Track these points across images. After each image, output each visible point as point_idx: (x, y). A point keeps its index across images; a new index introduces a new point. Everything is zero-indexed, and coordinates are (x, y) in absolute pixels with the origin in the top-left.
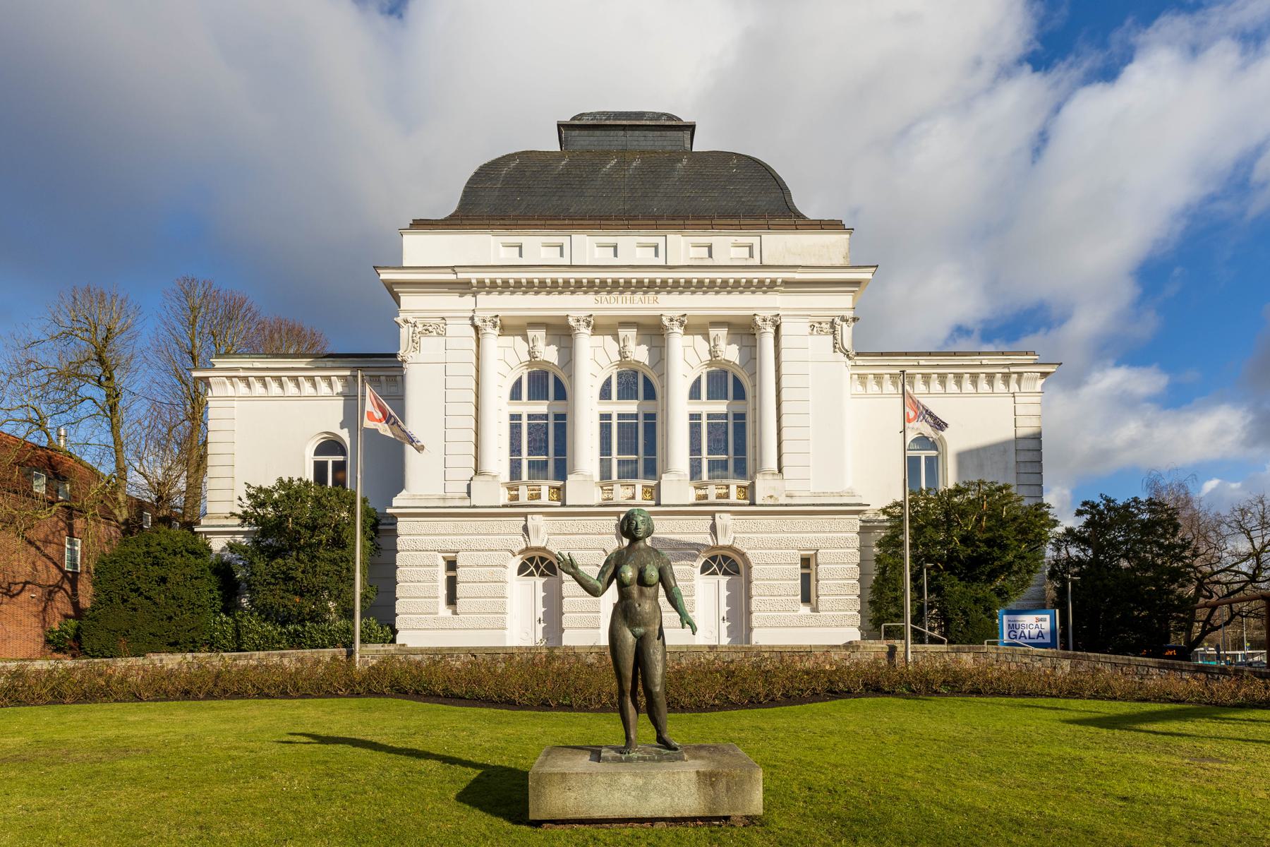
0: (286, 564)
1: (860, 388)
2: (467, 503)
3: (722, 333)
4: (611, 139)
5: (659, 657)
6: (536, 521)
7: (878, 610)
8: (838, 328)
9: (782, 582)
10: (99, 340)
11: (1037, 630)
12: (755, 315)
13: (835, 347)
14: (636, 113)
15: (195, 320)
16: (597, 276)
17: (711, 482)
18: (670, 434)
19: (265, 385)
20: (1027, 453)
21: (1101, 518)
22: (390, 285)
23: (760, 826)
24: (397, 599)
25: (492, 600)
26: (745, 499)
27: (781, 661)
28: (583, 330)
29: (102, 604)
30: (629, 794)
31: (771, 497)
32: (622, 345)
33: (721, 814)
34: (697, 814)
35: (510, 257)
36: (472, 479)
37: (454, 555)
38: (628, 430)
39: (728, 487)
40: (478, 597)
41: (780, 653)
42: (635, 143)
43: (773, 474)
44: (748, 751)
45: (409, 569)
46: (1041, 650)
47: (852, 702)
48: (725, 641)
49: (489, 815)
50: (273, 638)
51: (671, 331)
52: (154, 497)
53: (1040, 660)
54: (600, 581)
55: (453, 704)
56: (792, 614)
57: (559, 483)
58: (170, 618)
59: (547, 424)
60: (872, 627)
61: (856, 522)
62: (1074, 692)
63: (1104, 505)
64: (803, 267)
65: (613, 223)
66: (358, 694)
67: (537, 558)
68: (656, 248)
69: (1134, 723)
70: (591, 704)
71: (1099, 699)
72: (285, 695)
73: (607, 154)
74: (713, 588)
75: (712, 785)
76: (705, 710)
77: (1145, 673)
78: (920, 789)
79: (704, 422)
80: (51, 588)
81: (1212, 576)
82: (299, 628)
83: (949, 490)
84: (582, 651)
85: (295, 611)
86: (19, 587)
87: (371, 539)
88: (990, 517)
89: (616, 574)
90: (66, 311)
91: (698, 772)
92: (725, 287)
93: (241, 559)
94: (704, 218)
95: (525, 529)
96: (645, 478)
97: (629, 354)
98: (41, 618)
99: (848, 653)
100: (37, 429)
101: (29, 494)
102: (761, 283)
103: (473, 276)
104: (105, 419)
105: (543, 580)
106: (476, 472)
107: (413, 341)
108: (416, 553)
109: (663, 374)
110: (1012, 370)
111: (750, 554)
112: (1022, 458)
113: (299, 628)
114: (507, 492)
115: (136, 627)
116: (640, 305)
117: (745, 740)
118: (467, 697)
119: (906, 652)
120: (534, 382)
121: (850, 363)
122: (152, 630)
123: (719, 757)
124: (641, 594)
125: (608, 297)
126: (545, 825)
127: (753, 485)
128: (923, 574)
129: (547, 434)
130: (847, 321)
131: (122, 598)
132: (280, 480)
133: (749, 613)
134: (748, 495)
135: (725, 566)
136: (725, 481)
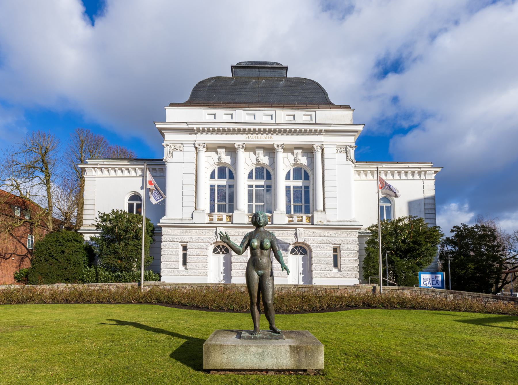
0: (115, 246)
1: (358, 176)
2: (191, 222)
3: (299, 152)
4: (253, 72)
5: (271, 286)
7: (367, 271)
8: (349, 150)
9: (325, 258)
10: (43, 153)
12: (313, 144)
13: (347, 158)
14: (263, 62)
15: (82, 146)
16: (247, 127)
17: (295, 214)
18: (277, 201)
19: (108, 171)
20: (429, 205)
21: (462, 233)
22: (160, 130)
23: (323, 375)
24: (161, 262)
26: (309, 222)
27: (326, 292)
28: (241, 150)
29: (37, 262)
30: (255, 357)
31: (320, 221)
32: (257, 156)
33: (302, 368)
34: (290, 368)
35: (211, 118)
36: (193, 212)
37: (186, 244)
39: (302, 217)
40: (195, 262)
41: (326, 289)
42: (263, 74)
43: (321, 212)
44: (313, 333)
45: (167, 249)
46: (440, 289)
47: (358, 311)
48: (301, 283)
49: (184, 365)
50: (109, 278)
51: (278, 151)
52: (64, 218)
53: (440, 294)
54: (241, 247)
55: (181, 308)
57: (230, 214)
58: (66, 269)
60: (364, 278)
61: (357, 233)
62: (457, 308)
63: (463, 228)
64: (333, 124)
65: (254, 105)
66: (141, 303)
68: (272, 116)
69: (492, 322)
70: (242, 310)
71: (468, 312)
72: (109, 302)
73: (251, 78)
75: (298, 352)
76: (293, 313)
77: (487, 300)
78: (401, 356)
80: (23, 256)
81: (506, 260)
83: (396, 220)
84: (239, 286)
85: (118, 267)
86: (9, 256)
87: (151, 236)
88: (414, 232)
89: (249, 244)
90: (29, 140)
91: (290, 346)
92: (300, 132)
93: (96, 244)
94: (292, 104)
97: (260, 160)
98: (18, 268)
99: (355, 289)
100: (16, 189)
101: (12, 216)
102: (316, 131)
103: (195, 127)
104: (44, 185)
105: (224, 255)
107: (170, 153)
108: (170, 243)
109: (274, 169)
110: (422, 169)
111: (311, 246)
112: (426, 207)
115: (51, 272)
116: (265, 140)
117: (311, 328)
118: (188, 305)
119: (380, 289)
121: (353, 165)
122: (58, 274)
123: (301, 338)
124: (262, 253)
125: (251, 136)
126: (212, 372)
127: (313, 216)
128: (386, 256)
130: (352, 147)
131: (46, 259)
132: (113, 210)
133: (311, 271)
134: (311, 220)
135: (301, 251)
136: (301, 214)
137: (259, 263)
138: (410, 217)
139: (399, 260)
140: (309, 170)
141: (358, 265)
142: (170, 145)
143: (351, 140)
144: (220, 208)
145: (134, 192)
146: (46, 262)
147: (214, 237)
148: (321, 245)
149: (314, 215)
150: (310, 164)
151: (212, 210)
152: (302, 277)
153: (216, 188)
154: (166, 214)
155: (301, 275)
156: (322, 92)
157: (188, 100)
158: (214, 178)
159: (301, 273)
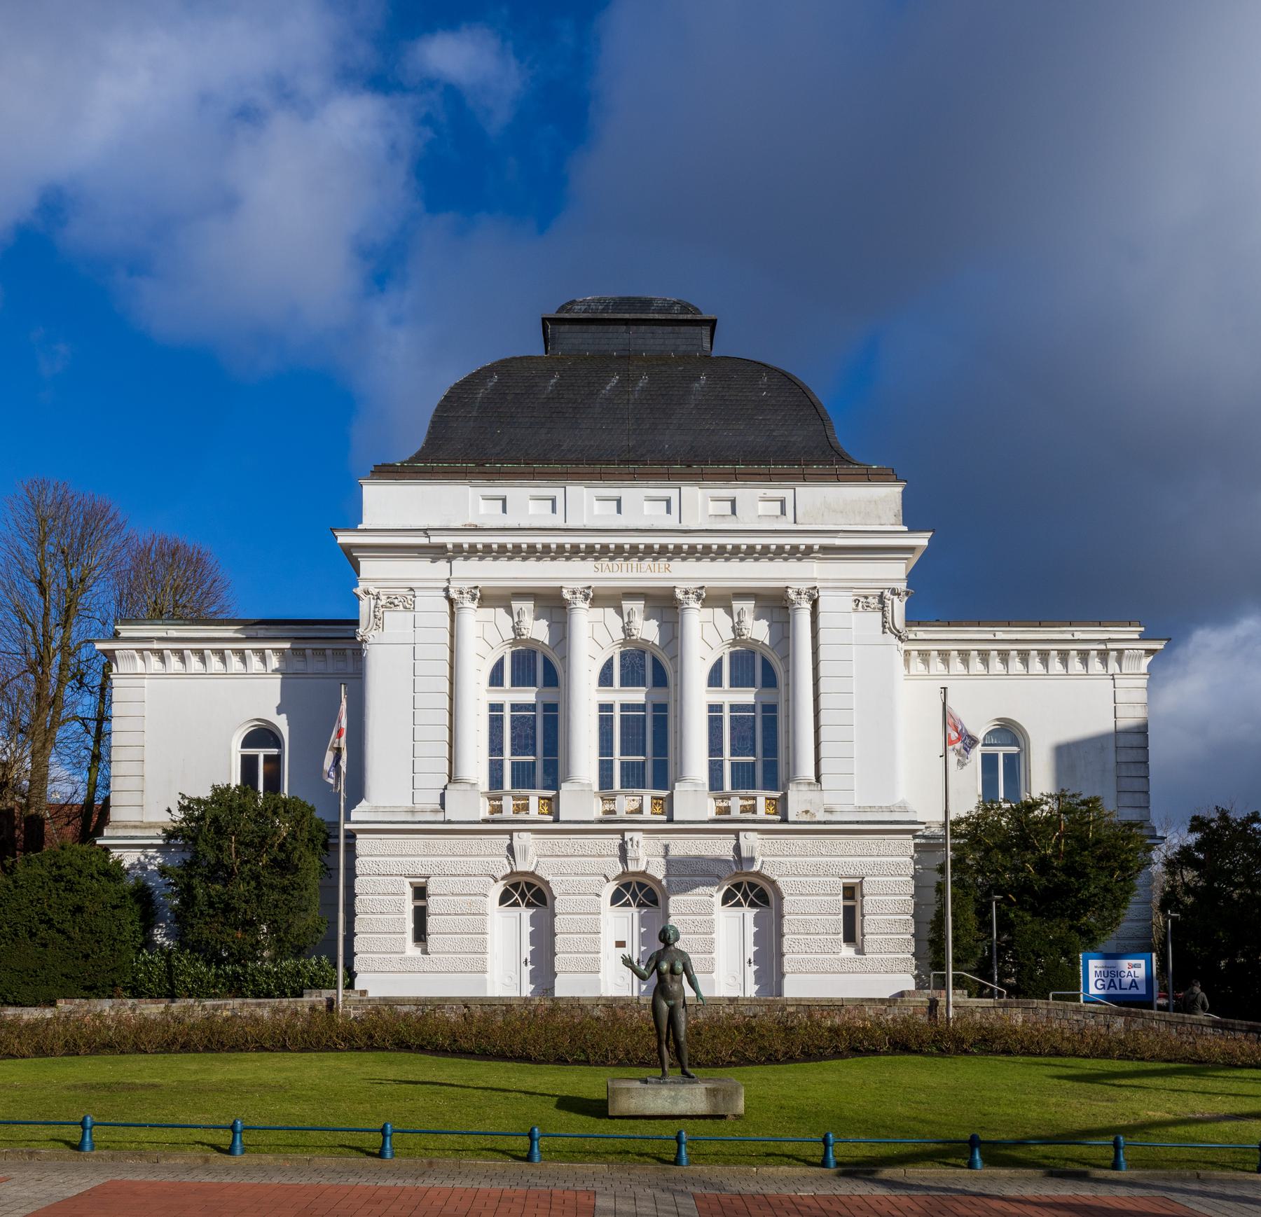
2: (440, 817)
6: (523, 840)
9: (819, 917)
11: (1130, 979)
12: (787, 587)
13: (884, 627)
22: (348, 549)
25: (469, 936)
31: (807, 812)
36: (445, 788)
37: (424, 880)
38: (632, 726)
39: (755, 798)
41: (808, 1006)
42: (640, 341)
43: (810, 784)
45: (370, 897)
48: (751, 990)
51: (687, 606)
53: (1093, 1017)
56: (832, 956)
57: (550, 793)
58: (86, 956)
59: (535, 715)
67: (523, 884)
74: (737, 923)
75: (715, 1096)
76: (722, 1066)
77: (1199, 1032)
79: (726, 715)
82: (239, 970)
84: (587, 1002)
89: (657, 966)
95: (510, 849)
96: (655, 788)
103: (449, 540)
105: (531, 911)
106: (450, 777)
107: (375, 616)
108: (379, 878)
110: (1110, 646)
111: (781, 882)
112: (1123, 758)
113: (239, 970)
114: (488, 803)
116: (649, 575)
120: (518, 663)
122: (65, 971)
124: (672, 979)
125: (610, 564)
128: (991, 908)
129: (534, 728)
130: (899, 594)
133: (781, 955)
134: (779, 808)
136: (751, 792)
137: (669, 992)
138: (1059, 797)
139: (1029, 918)
140: (777, 660)
141: (913, 935)
142: (374, 591)
143: (895, 572)
144: (518, 771)
145: (258, 720)
146: (30, 937)
147: (506, 861)
148: (807, 879)
149: (789, 793)
150: (780, 641)
151: (496, 781)
152: (755, 972)
153: (507, 714)
154: (367, 795)
155: (752, 964)
156: (817, 417)
157: (423, 448)
158: (502, 685)
159: (752, 961)
